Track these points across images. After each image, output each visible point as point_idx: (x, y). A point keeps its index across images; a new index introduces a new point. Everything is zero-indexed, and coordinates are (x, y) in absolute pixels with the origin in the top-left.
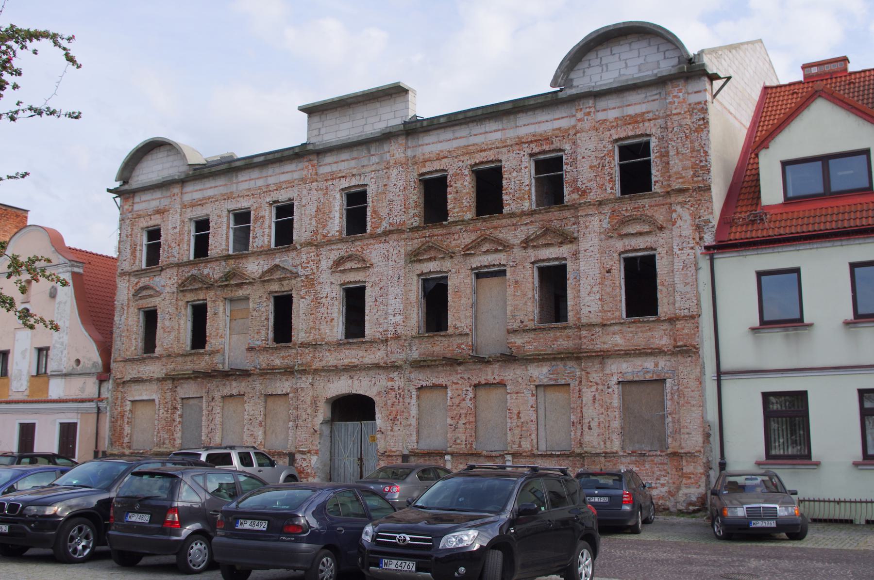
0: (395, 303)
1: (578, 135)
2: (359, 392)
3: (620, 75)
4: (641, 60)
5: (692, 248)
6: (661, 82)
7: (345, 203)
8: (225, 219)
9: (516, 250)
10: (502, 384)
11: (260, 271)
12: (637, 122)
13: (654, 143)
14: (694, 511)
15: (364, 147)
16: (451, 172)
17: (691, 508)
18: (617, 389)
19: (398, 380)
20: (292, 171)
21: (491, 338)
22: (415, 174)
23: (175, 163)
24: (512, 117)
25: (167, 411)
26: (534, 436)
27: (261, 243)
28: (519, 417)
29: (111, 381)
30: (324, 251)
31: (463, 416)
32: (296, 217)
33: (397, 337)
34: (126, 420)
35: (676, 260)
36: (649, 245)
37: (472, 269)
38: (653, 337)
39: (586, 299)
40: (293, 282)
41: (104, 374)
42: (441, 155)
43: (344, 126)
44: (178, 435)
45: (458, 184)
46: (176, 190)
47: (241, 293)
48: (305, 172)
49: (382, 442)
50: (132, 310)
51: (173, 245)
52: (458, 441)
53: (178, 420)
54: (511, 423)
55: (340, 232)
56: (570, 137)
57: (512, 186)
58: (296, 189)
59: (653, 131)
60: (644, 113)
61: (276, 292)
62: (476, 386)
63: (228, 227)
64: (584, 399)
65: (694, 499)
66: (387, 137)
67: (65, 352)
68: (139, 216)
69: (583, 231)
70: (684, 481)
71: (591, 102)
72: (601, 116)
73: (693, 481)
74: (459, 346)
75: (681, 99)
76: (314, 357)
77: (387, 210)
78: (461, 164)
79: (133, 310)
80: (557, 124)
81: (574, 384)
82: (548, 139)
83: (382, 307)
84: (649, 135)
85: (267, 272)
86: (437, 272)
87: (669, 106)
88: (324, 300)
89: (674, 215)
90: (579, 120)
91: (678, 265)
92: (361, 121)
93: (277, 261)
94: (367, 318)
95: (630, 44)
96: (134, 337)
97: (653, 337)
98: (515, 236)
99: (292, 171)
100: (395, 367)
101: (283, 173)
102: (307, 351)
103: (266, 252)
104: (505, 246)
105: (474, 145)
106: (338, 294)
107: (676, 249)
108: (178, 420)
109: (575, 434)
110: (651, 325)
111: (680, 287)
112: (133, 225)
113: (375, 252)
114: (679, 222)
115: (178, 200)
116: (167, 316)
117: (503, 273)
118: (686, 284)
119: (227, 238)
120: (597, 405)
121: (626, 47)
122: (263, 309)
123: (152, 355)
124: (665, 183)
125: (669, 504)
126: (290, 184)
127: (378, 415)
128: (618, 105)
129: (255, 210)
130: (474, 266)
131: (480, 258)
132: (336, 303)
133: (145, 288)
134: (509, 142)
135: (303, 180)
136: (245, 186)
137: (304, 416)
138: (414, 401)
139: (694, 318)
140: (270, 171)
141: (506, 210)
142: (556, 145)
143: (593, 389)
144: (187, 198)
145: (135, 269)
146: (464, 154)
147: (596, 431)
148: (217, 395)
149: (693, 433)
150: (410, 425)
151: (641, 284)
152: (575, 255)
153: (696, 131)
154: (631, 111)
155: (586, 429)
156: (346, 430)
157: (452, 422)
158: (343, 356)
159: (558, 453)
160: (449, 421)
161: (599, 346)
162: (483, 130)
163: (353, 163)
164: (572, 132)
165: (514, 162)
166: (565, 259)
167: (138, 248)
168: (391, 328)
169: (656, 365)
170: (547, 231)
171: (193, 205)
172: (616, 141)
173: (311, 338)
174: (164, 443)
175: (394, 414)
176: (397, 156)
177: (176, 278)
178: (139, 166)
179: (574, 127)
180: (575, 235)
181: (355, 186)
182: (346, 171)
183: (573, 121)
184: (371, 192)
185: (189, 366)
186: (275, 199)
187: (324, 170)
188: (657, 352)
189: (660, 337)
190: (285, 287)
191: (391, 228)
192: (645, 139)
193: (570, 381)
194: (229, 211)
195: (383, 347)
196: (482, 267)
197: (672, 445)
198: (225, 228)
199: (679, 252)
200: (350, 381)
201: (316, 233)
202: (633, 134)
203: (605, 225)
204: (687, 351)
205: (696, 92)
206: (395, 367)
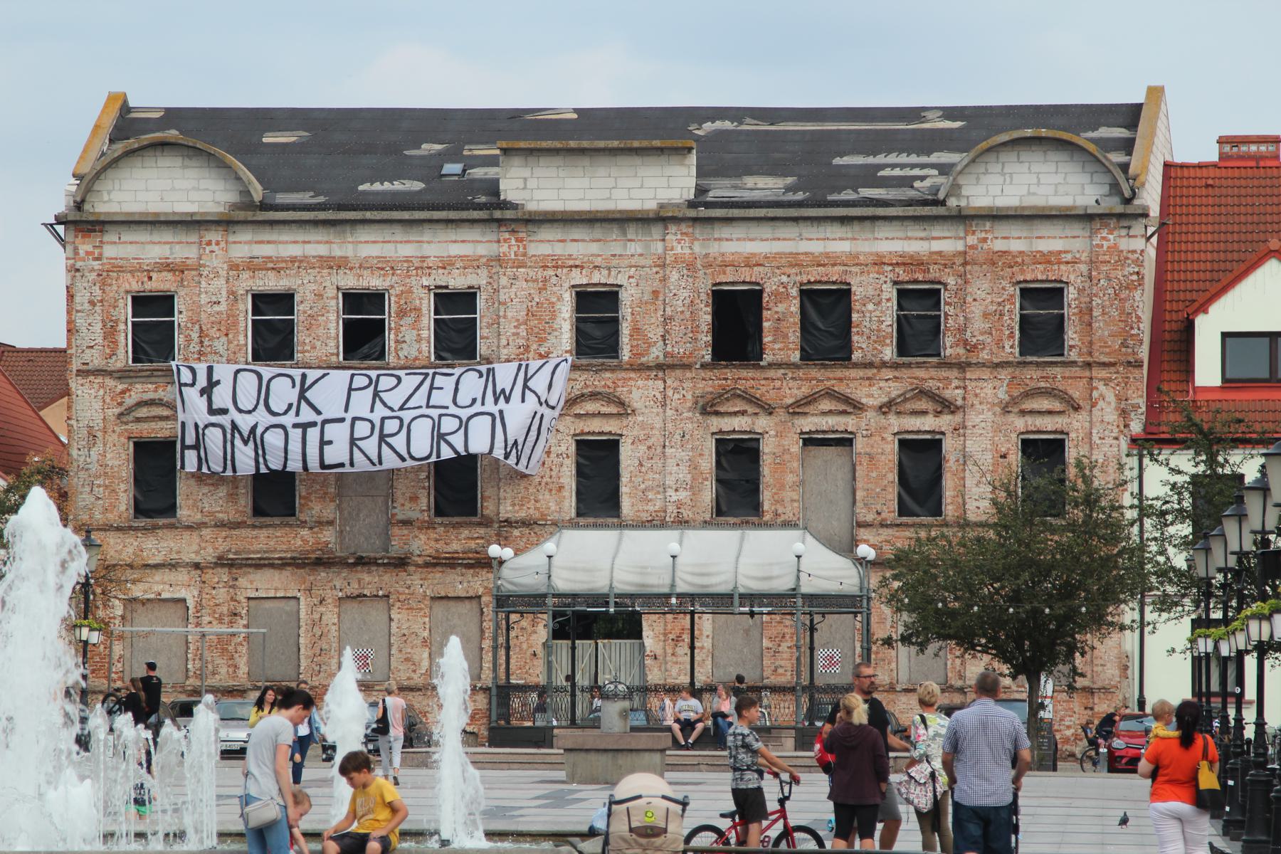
0: (677, 472)
1: (968, 267)
6: (1087, 218)
10: (845, 442)
12: (1049, 262)
27: (414, 353)
31: (788, 637)
36: (1059, 426)
37: (802, 433)
46: (214, 235)
51: (213, 332)
57: (867, 324)
58: (484, 273)
68: (121, 269)
69: (971, 399)
77: (660, 331)
78: (784, 279)
98: (872, 393)
107: (1095, 438)
114: (1101, 403)
126: (471, 263)
146: (792, 265)
149: (1109, 665)
152: (959, 429)
160: (766, 643)
166: (943, 433)
171: (254, 266)
180: (959, 402)
183: (960, 246)
196: (817, 432)
199: (1098, 442)
202: (1044, 277)
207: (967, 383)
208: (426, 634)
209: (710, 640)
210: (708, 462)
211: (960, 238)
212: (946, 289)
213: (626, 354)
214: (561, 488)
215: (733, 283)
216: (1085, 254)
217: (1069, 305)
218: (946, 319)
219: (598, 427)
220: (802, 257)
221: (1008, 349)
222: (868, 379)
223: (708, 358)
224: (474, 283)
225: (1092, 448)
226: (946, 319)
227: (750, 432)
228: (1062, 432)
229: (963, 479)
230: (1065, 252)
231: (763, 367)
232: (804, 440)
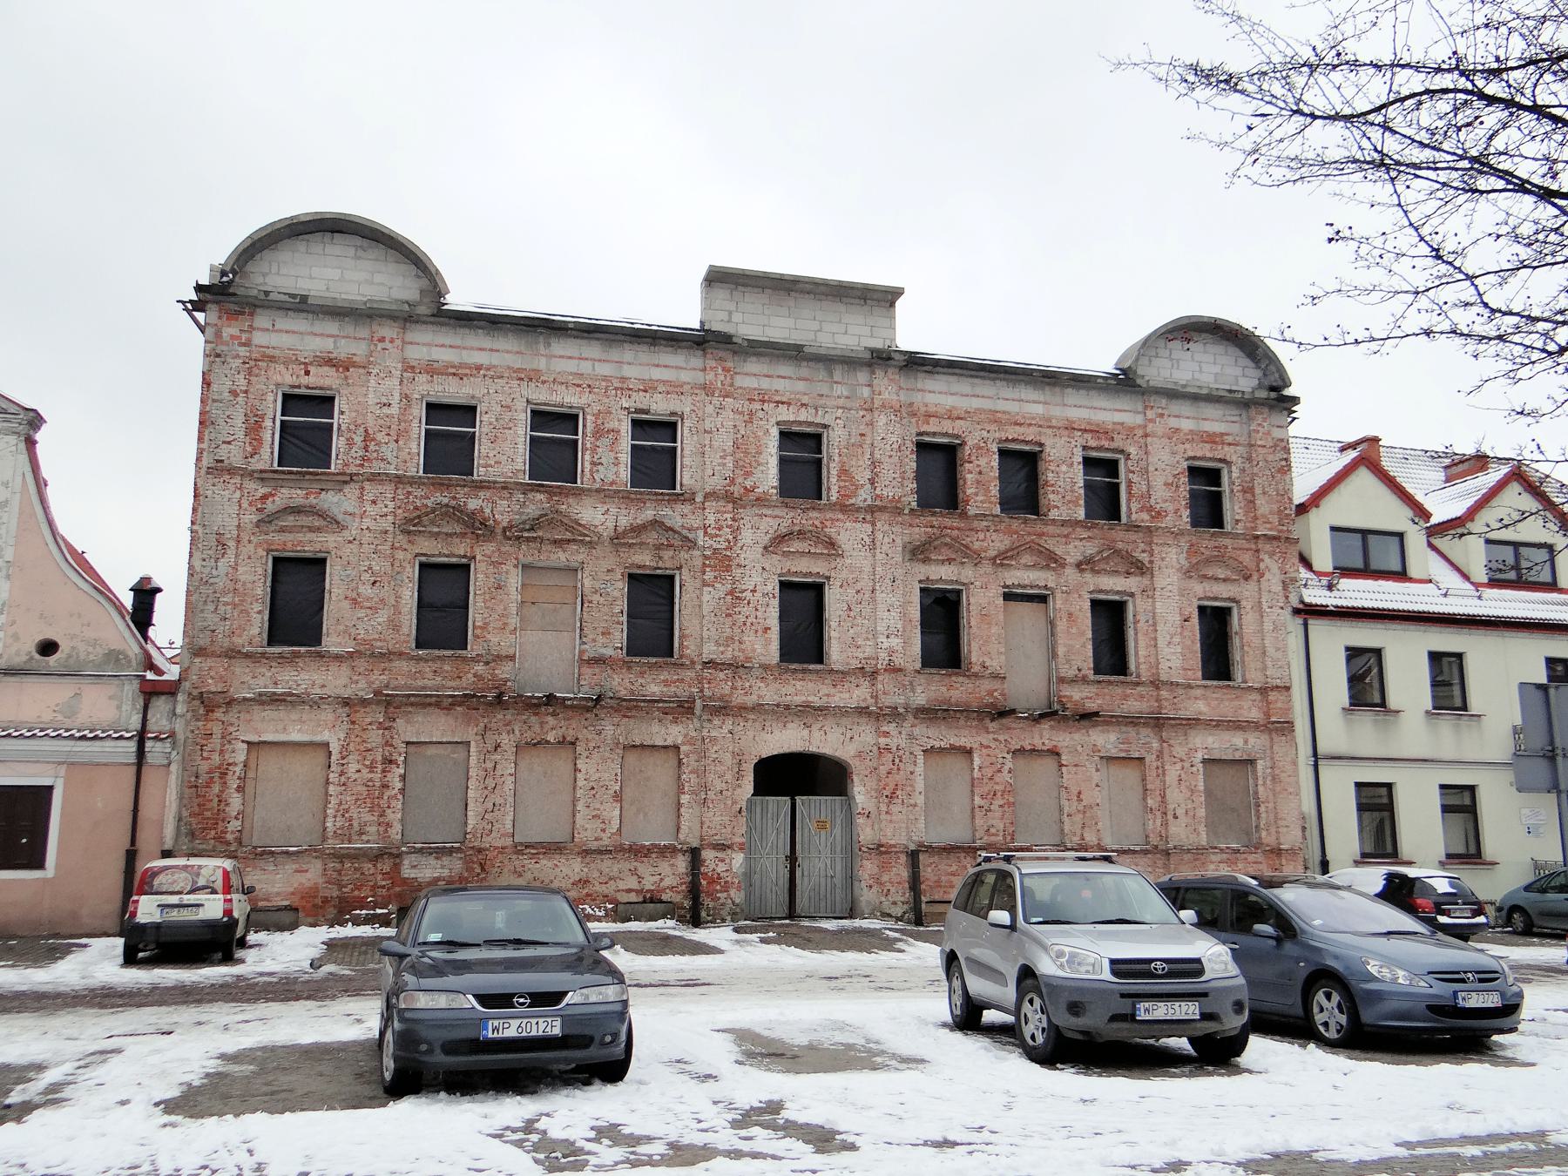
4: (1217, 369)
10: (1055, 753)
12: (1215, 442)
16: (971, 442)
19: (896, 736)
21: (1026, 684)
22: (914, 431)
23: (378, 278)
24: (1057, 389)
27: (611, 477)
28: (1080, 800)
30: (748, 515)
36: (1231, 594)
37: (1006, 586)
38: (1241, 708)
39: (1165, 651)
40: (684, 555)
42: (955, 414)
43: (776, 321)
44: (394, 816)
45: (983, 462)
46: (388, 331)
47: (561, 557)
48: (710, 376)
49: (868, 830)
50: (248, 549)
51: (380, 437)
52: (993, 830)
59: (1234, 458)
60: (1222, 434)
66: (849, 362)
69: (1156, 559)
72: (1173, 423)
74: (990, 693)
76: (734, 688)
77: (868, 474)
78: (985, 434)
80: (1118, 417)
81: (1150, 759)
83: (859, 620)
88: (748, 594)
90: (1151, 421)
91: (1268, 626)
97: (1241, 708)
100: (894, 714)
102: (722, 675)
104: (1052, 561)
109: (1155, 824)
111: (1271, 651)
114: (1267, 576)
126: (676, 389)
130: (1009, 583)
131: (1018, 573)
134: (1054, 423)
137: (719, 785)
139: (1288, 688)
140: (628, 353)
142: (1118, 443)
143: (1178, 766)
144: (416, 354)
145: (260, 466)
147: (1183, 820)
148: (506, 741)
155: (1170, 817)
157: (982, 803)
158: (791, 690)
160: (978, 801)
161: (1182, 714)
163: (801, 386)
165: (1063, 452)
169: (1246, 742)
171: (432, 370)
173: (729, 655)
175: (892, 786)
176: (886, 396)
181: (800, 423)
182: (796, 397)
183: (1139, 420)
185: (407, 675)
187: (743, 382)
188: (1237, 726)
190: (667, 562)
197: (1268, 838)
200: (806, 732)
204: (1287, 727)
206: (894, 714)
214: (767, 629)
215: (934, 434)
219: (805, 568)
224: (678, 410)
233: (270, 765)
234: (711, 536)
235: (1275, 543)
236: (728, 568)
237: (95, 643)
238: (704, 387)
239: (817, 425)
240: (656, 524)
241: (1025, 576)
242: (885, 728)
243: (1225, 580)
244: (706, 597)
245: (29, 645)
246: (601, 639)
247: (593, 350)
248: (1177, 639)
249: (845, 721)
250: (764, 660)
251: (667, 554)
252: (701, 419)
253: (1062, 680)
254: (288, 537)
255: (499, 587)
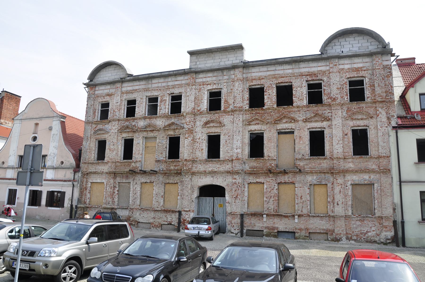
0: (237, 143)
1: (331, 74)
2: (216, 184)
3: (350, 50)
4: (360, 45)
5: (387, 127)
6: (371, 55)
7: (209, 96)
8: (145, 100)
9: (300, 122)
10: (293, 183)
11: (163, 125)
12: (358, 71)
13: (366, 81)
14: (389, 243)
15: (220, 71)
17: (388, 241)
18: (350, 187)
19: (239, 179)
20: (183, 80)
23: (118, 73)
24: (297, 64)
25: (111, 188)
26: (309, 207)
27: (164, 112)
28: (301, 198)
29: (80, 172)
30: (198, 118)
31: (272, 197)
32: (183, 101)
33: (237, 159)
34: (88, 191)
35: (379, 131)
36: (365, 124)
37: (277, 130)
39: (336, 146)
40: (181, 131)
41: (77, 168)
42: (261, 78)
43: (208, 62)
44: (116, 200)
45: (270, 91)
46: (119, 85)
49: (229, 208)
50: (92, 139)
51: (116, 110)
52: (270, 208)
53: (117, 192)
54: (298, 201)
55: (207, 109)
56: (326, 75)
57: (298, 94)
58: (183, 88)
59: (367, 75)
61: (171, 135)
62: (279, 183)
63: (146, 104)
64: (335, 191)
65: (389, 237)
66: (234, 67)
67: (56, 158)
68: (98, 97)
69: (334, 115)
70: (384, 229)
71: (337, 60)
72: (341, 67)
73: (388, 229)
75: (380, 63)
76: (192, 166)
77: (233, 101)
78: (271, 82)
79: (93, 140)
80: (319, 69)
81: (329, 185)
82: (315, 75)
83: (229, 145)
84: (365, 77)
85: (167, 125)
86: (259, 130)
87: (374, 65)
88: (198, 140)
89: (378, 112)
91: (380, 134)
92: (218, 60)
93: (173, 121)
94: (221, 149)
95: (354, 37)
96: (93, 152)
98: (300, 116)
99: (181, 80)
100: (237, 173)
101: (177, 81)
103: (165, 116)
104: (294, 120)
105: (278, 74)
106: (205, 138)
107: (379, 127)
108: (117, 192)
110: (367, 159)
111: (381, 143)
112: (94, 100)
113: (226, 119)
114: (380, 115)
115: (120, 90)
116: (112, 144)
117: (293, 133)
118: (384, 142)
119: (145, 109)
120: (341, 194)
121: (352, 39)
122: (164, 143)
123: (103, 161)
124: (373, 98)
125: (377, 239)
126: (180, 86)
127: (227, 195)
128: (349, 63)
129: (161, 97)
130: (278, 128)
132: (205, 141)
133: (100, 130)
134: (296, 75)
135: (188, 84)
136: (156, 85)
137: (187, 194)
138: (246, 189)
139: (388, 157)
141: (294, 104)
143: (340, 187)
144: (124, 89)
145: (95, 121)
146: (273, 78)
147: (341, 206)
149: (388, 208)
150: (244, 200)
151: (360, 141)
152: (330, 126)
153: (387, 77)
154: (356, 66)
155: (335, 204)
156: (206, 201)
159: (322, 215)
160: (265, 199)
162: (282, 68)
163: (214, 78)
164: (327, 72)
165: (299, 84)
166: (325, 128)
167: (97, 111)
168: (235, 155)
169: (370, 177)
170: (316, 115)
171: (127, 92)
172: (348, 78)
174: (109, 203)
175: (236, 194)
176: (238, 76)
177: (117, 126)
178: (99, 74)
179: (329, 70)
180: (330, 117)
181: (214, 89)
182: (212, 82)
183: (328, 68)
184: (224, 92)
186: (172, 92)
188: (373, 171)
189: (372, 165)
190: (176, 134)
191: (235, 109)
192: (362, 78)
193: (327, 183)
194: (147, 97)
195: (230, 164)
196: (282, 129)
198: (144, 104)
199: (380, 128)
200: (212, 179)
201: (194, 109)
202: (357, 76)
203: (344, 114)
204: (387, 171)
205: (386, 61)
206: (237, 173)
207: (332, 111)
208: (163, 194)
209: (247, 198)
210: (247, 140)
211: (328, 66)
212: (324, 82)
213: (222, 108)
214: (202, 150)
215: (255, 85)
216: (370, 67)
217: (366, 84)
218: (324, 91)
219: (214, 131)
220: (276, 75)
221: (346, 99)
222: (299, 111)
223: (247, 108)
224: (181, 92)
225: (378, 130)
226: (324, 91)
227: (260, 130)
228: (366, 126)
229: (332, 143)
230: (363, 67)
231: (264, 110)
232: (278, 132)
233: (95, 187)
234: (188, 125)
235: (384, 103)
236: (192, 133)
237: (69, 162)
238: (187, 84)
239: (219, 89)
240: (173, 124)
241: (284, 126)
242: (235, 177)
243: (362, 119)
244: (186, 142)
245: (59, 163)
246: (160, 155)
247: (162, 80)
248: (341, 142)
249: (223, 175)
250: (201, 158)
251: (177, 131)
252: (186, 93)
253: (296, 159)
254: (99, 136)
255: (138, 144)
